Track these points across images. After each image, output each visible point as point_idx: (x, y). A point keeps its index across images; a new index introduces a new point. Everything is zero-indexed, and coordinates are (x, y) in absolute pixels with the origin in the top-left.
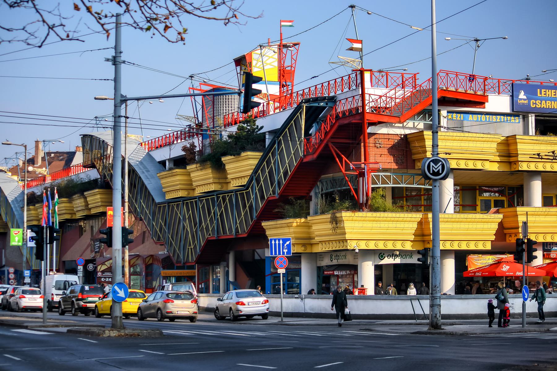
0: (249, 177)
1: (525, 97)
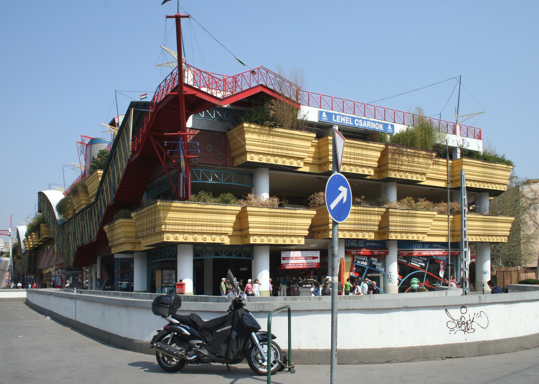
0: (95, 196)
1: (326, 116)
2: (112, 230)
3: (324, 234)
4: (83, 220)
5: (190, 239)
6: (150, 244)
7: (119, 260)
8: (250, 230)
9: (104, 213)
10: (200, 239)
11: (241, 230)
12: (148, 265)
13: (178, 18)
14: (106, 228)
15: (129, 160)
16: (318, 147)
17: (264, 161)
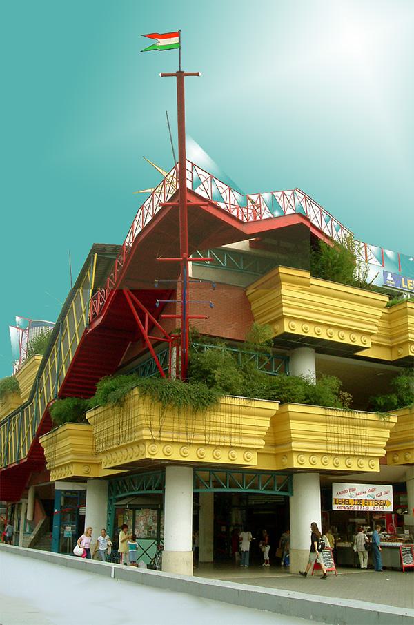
1: (392, 279)
2: (52, 443)
3: (407, 456)
4: (9, 430)
5: (192, 456)
6: (118, 464)
7: (63, 493)
8: (293, 444)
9: (41, 417)
10: (208, 457)
11: (276, 445)
12: (110, 501)
13: (180, 76)
14: (43, 440)
15: (86, 331)
16: (388, 319)
17: (311, 334)
